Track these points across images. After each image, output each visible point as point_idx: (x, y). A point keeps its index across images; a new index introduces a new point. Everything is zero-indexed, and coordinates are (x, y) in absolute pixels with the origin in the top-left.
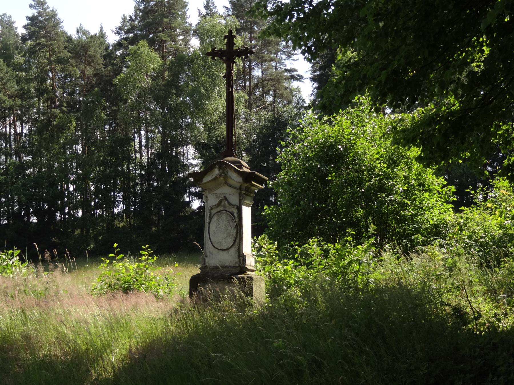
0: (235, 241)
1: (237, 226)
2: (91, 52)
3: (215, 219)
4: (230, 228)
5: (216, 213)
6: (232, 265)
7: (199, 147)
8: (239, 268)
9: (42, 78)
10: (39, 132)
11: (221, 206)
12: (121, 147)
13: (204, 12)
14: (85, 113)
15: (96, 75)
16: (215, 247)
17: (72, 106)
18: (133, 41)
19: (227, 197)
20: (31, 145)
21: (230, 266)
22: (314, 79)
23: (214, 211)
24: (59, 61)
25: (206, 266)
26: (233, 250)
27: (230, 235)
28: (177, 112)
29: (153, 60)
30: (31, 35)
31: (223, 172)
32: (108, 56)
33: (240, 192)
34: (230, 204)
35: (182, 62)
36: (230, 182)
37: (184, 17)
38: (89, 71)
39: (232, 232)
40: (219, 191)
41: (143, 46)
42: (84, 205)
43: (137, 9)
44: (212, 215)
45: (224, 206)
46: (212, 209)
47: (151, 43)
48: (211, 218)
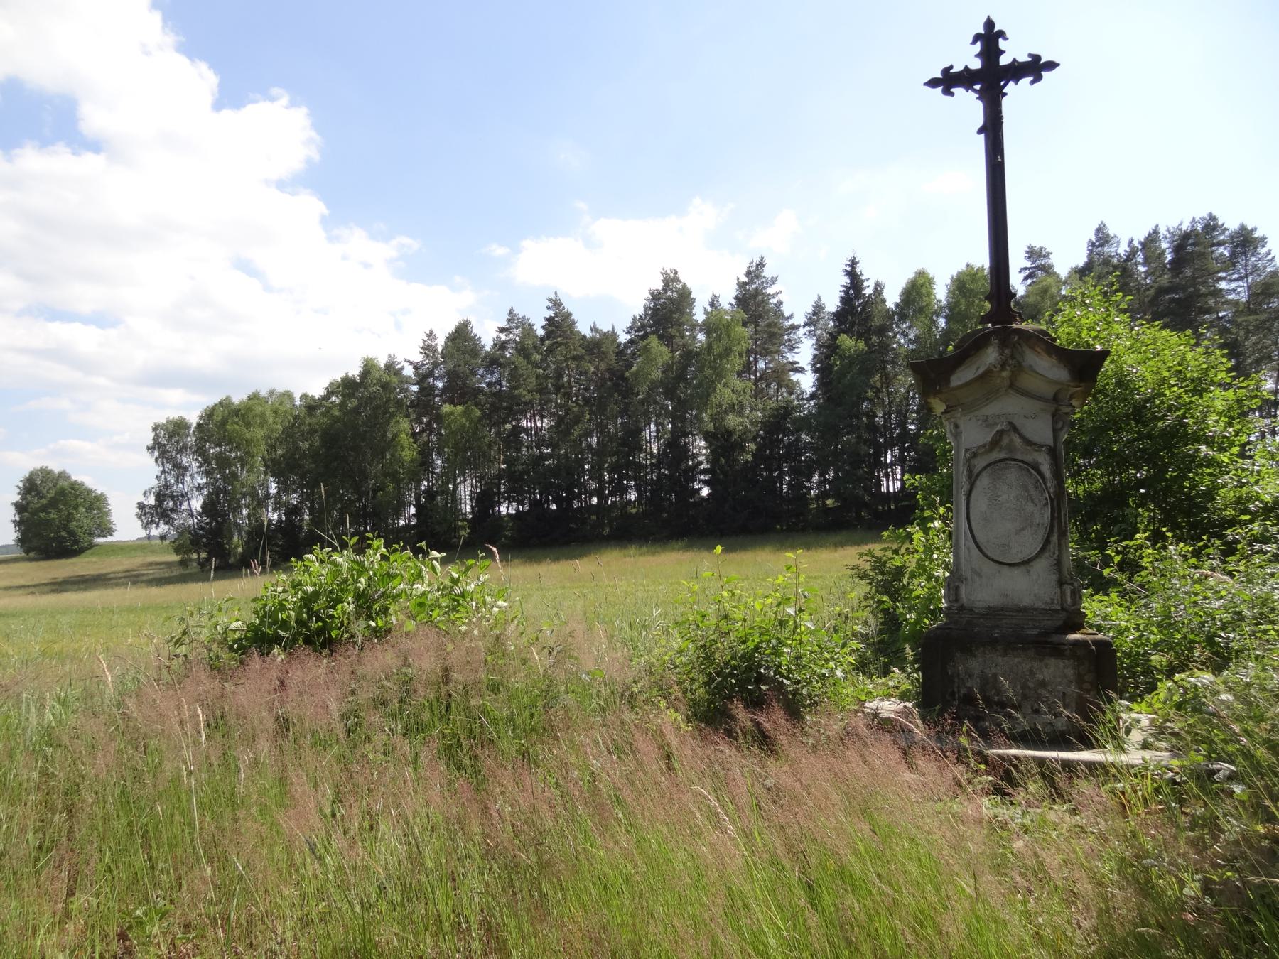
1: (1052, 500)
2: (604, 349)
3: (984, 482)
5: (988, 465)
6: (1039, 604)
7: (707, 436)
8: (1063, 615)
9: (559, 374)
10: (558, 424)
12: (632, 440)
13: (709, 309)
14: (598, 407)
15: (609, 370)
16: (987, 556)
17: (587, 401)
18: (643, 338)
19: (1019, 426)
20: (551, 438)
21: (1036, 609)
22: (815, 371)
23: (980, 463)
24: (575, 358)
25: (962, 608)
26: (1042, 565)
27: (1031, 525)
28: (682, 405)
29: (661, 352)
30: (549, 335)
31: (1012, 357)
32: (620, 353)
33: (1057, 410)
34: (1028, 442)
35: (689, 355)
36: (1027, 381)
37: (691, 314)
38: (603, 367)
40: (991, 409)
41: (653, 340)
42: (599, 492)
43: (646, 308)
44: (976, 471)
45: (1010, 448)
46: (975, 455)
47: (661, 338)
48: (973, 478)
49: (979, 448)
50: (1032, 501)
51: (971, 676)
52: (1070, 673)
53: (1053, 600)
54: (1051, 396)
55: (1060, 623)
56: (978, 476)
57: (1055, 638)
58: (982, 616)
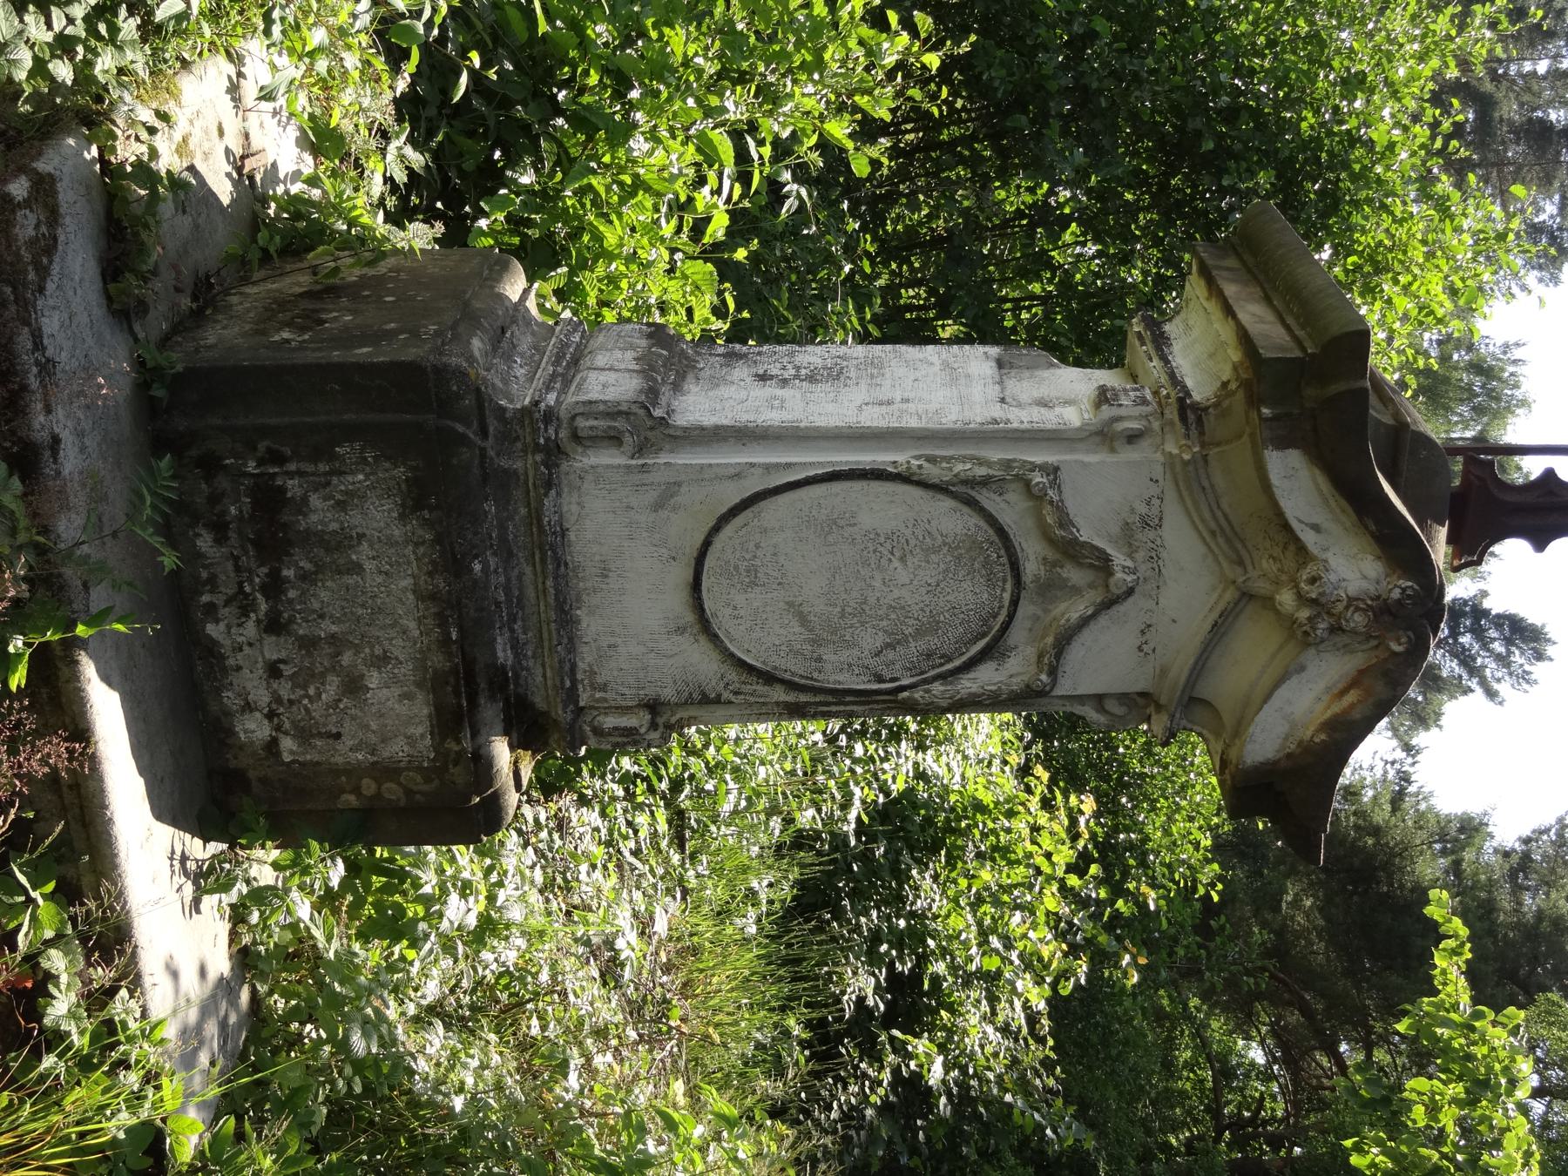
0: (769, 678)
3: (949, 519)
4: (870, 640)
5: (1001, 532)
6: (586, 658)
8: (563, 715)
11: (1051, 565)
16: (716, 529)
21: (572, 648)
25: (554, 453)
26: (702, 664)
27: (816, 642)
31: (1336, 629)
34: (1064, 640)
39: (846, 655)
40: (1180, 540)
44: (987, 499)
45: (1051, 588)
46: (1035, 496)
49: (1060, 509)
50: (887, 645)
51: (341, 506)
52: (397, 749)
53: (604, 687)
54: (1204, 690)
55: (539, 701)
56: (971, 503)
57: (490, 711)
58: (536, 515)
